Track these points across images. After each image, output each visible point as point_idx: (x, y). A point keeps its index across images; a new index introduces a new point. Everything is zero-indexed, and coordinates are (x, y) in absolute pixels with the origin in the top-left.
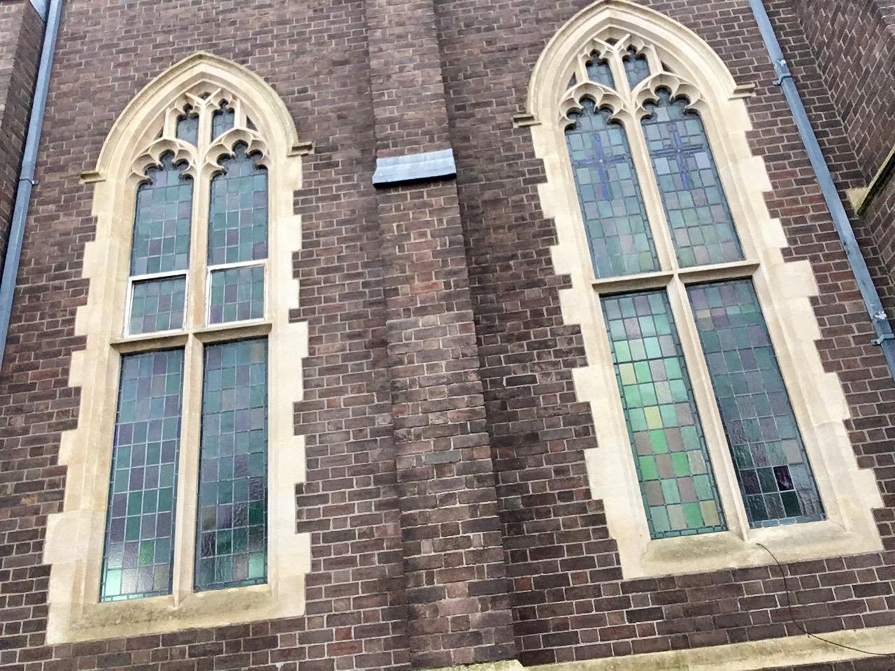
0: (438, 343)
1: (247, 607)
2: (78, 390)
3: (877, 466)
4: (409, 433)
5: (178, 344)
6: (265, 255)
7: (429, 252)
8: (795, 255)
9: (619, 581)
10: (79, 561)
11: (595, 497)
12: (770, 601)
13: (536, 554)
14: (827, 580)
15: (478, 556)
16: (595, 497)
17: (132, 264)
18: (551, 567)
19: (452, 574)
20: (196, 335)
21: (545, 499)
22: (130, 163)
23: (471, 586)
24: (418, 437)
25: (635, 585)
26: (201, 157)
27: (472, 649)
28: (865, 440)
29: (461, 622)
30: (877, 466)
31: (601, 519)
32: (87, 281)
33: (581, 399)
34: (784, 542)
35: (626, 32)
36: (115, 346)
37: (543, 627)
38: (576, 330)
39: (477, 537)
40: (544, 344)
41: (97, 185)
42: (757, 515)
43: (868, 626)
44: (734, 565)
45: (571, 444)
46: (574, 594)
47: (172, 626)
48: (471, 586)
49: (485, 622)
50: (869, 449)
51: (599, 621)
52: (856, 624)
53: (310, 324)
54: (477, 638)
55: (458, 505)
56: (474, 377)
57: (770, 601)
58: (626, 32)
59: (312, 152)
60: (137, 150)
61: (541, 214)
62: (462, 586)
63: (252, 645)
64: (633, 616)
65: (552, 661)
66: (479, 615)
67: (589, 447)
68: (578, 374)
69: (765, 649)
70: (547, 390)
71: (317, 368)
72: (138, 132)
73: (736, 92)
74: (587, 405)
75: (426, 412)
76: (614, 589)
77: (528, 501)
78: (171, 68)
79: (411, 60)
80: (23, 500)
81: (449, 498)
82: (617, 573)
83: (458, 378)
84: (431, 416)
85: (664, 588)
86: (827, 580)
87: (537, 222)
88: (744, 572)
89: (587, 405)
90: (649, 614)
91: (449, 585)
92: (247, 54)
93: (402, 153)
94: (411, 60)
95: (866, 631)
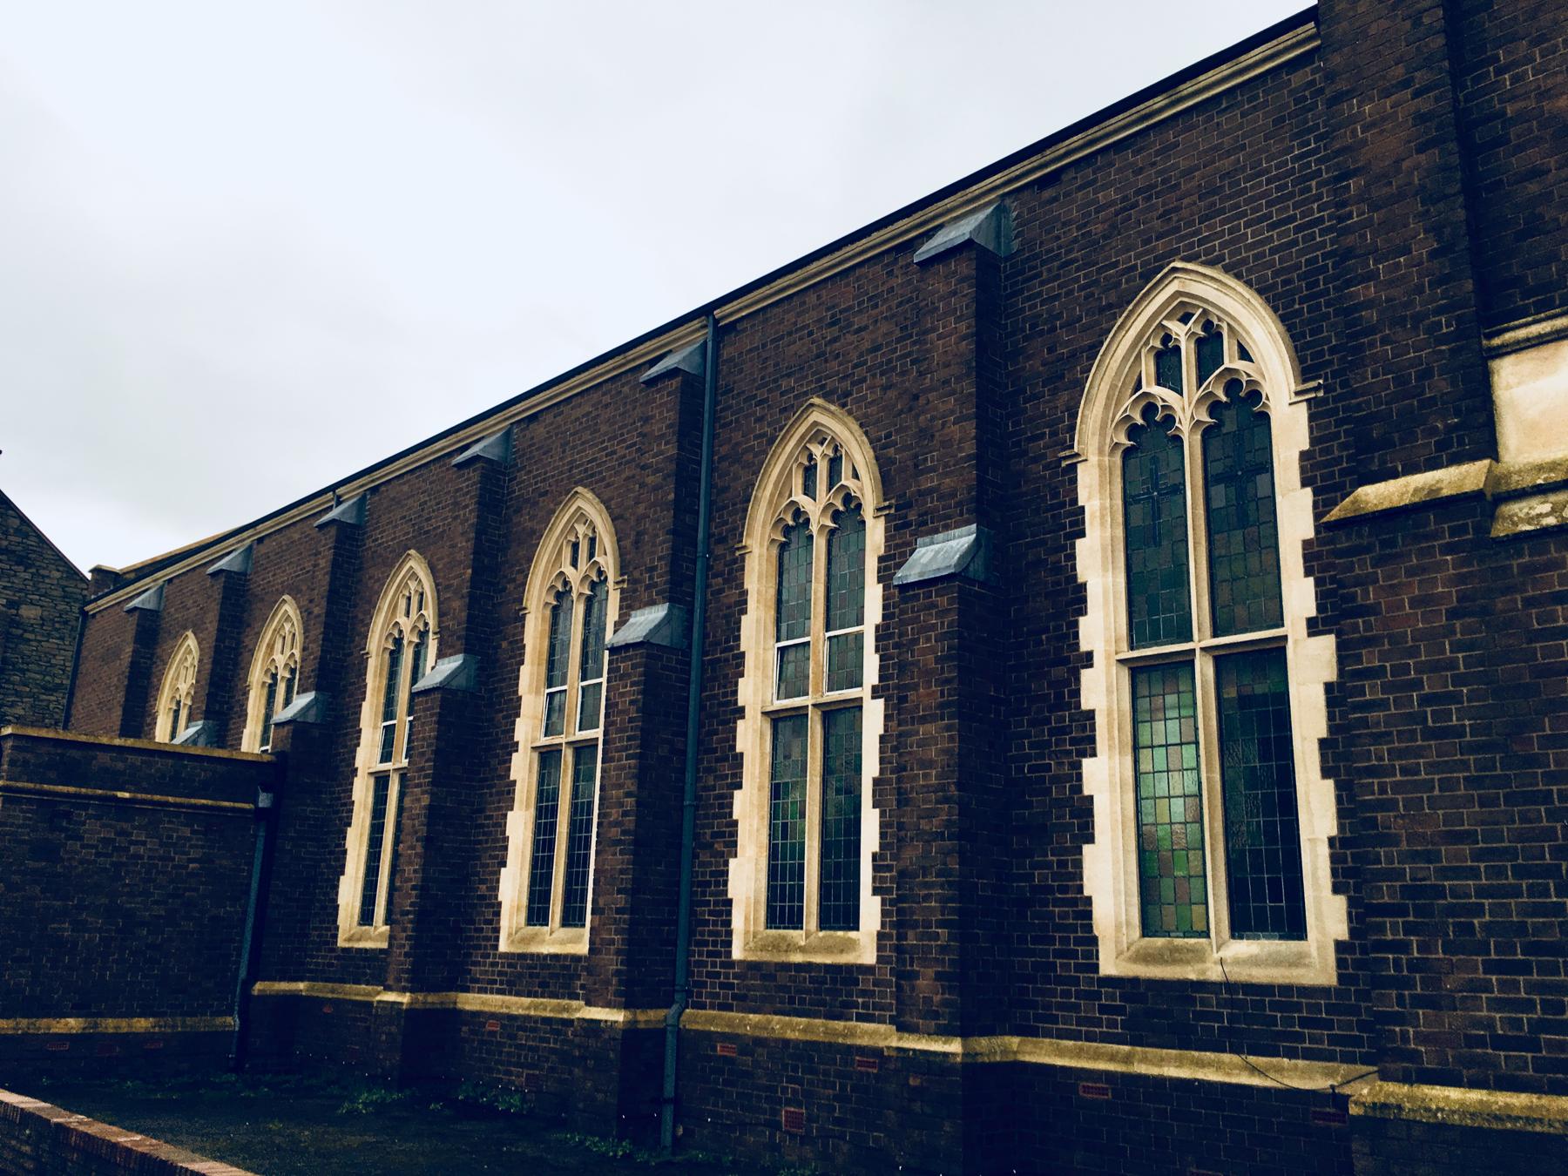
0: (932, 753)
1: (842, 951)
2: (742, 754)
3: (1352, 893)
4: (906, 835)
6: (863, 624)
7: (931, 657)
8: (1321, 628)
9: (1096, 976)
10: (748, 898)
11: (1086, 893)
12: (1218, 1017)
13: (1035, 940)
14: (1276, 1006)
15: (943, 949)
16: (1086, 893)
17: (778, 631)
18: (1045, 953)
19: (925, 961)
20: (814, 705)
21: (1050, 890)
22: (769, 528)
23: (937, 973)
24: (912, 839)
25: (1111, 981)
27: (933, 1023)
28: (1346, 862)
29: (928, 1000)
30: (1352, 893)
32: (744, 653)
33: (1086, 792)
34: (1254, 961)
35: (1199, 307)
36: (765, 714)
37: (1034, 1005)
38: (1091, 715)
40: (1063, 731)
41: (747, 556)
42: (1241, 927)
43: (1305, 1058)
44: (1193, 976)
45: (1074, 837)
46: (1060, 980)
47: (798, 958)
48: (937, 973)
49: (945, 1003)
50: (1348, 873)
51: (1076, 1008)
52: (1292, 1054)
53: (886, 701)
55: (933, 904)
56: (953, 788)
57: (1218, 1017)
58: (1199, 307)
59: (893, 511)
60: (774, 512)
61: (1075, 576)
62: (931, 972)
63: (845, 982)
65: (1037, 1035)
66: (939, 997)
67: (1088, 843)
68: (1087, 764)
69: (1202, 1061)
70: (1057, 779)
71: (889, 745)
72: (772, 495)
73: (1297, 393)
74: (1091, 798)
75: (920, 818)
76: (1090, 981)
77: (1034, 889)
78: (793, 419)
79: (952, 412)
80: (716, 846)
81: (927, 898)
82: (1095, 968)
83: (943, 788)
84: (921, 821)
85: (1128, 986)
86: (1276, 1006)
87: (1070, 587)
88: (1202, 985)
89: (1091, 798)
90: (1118, 1010)
91: (922, 970)
92: (847, 394)
94: (952, 412)
95: (1300, 1063)
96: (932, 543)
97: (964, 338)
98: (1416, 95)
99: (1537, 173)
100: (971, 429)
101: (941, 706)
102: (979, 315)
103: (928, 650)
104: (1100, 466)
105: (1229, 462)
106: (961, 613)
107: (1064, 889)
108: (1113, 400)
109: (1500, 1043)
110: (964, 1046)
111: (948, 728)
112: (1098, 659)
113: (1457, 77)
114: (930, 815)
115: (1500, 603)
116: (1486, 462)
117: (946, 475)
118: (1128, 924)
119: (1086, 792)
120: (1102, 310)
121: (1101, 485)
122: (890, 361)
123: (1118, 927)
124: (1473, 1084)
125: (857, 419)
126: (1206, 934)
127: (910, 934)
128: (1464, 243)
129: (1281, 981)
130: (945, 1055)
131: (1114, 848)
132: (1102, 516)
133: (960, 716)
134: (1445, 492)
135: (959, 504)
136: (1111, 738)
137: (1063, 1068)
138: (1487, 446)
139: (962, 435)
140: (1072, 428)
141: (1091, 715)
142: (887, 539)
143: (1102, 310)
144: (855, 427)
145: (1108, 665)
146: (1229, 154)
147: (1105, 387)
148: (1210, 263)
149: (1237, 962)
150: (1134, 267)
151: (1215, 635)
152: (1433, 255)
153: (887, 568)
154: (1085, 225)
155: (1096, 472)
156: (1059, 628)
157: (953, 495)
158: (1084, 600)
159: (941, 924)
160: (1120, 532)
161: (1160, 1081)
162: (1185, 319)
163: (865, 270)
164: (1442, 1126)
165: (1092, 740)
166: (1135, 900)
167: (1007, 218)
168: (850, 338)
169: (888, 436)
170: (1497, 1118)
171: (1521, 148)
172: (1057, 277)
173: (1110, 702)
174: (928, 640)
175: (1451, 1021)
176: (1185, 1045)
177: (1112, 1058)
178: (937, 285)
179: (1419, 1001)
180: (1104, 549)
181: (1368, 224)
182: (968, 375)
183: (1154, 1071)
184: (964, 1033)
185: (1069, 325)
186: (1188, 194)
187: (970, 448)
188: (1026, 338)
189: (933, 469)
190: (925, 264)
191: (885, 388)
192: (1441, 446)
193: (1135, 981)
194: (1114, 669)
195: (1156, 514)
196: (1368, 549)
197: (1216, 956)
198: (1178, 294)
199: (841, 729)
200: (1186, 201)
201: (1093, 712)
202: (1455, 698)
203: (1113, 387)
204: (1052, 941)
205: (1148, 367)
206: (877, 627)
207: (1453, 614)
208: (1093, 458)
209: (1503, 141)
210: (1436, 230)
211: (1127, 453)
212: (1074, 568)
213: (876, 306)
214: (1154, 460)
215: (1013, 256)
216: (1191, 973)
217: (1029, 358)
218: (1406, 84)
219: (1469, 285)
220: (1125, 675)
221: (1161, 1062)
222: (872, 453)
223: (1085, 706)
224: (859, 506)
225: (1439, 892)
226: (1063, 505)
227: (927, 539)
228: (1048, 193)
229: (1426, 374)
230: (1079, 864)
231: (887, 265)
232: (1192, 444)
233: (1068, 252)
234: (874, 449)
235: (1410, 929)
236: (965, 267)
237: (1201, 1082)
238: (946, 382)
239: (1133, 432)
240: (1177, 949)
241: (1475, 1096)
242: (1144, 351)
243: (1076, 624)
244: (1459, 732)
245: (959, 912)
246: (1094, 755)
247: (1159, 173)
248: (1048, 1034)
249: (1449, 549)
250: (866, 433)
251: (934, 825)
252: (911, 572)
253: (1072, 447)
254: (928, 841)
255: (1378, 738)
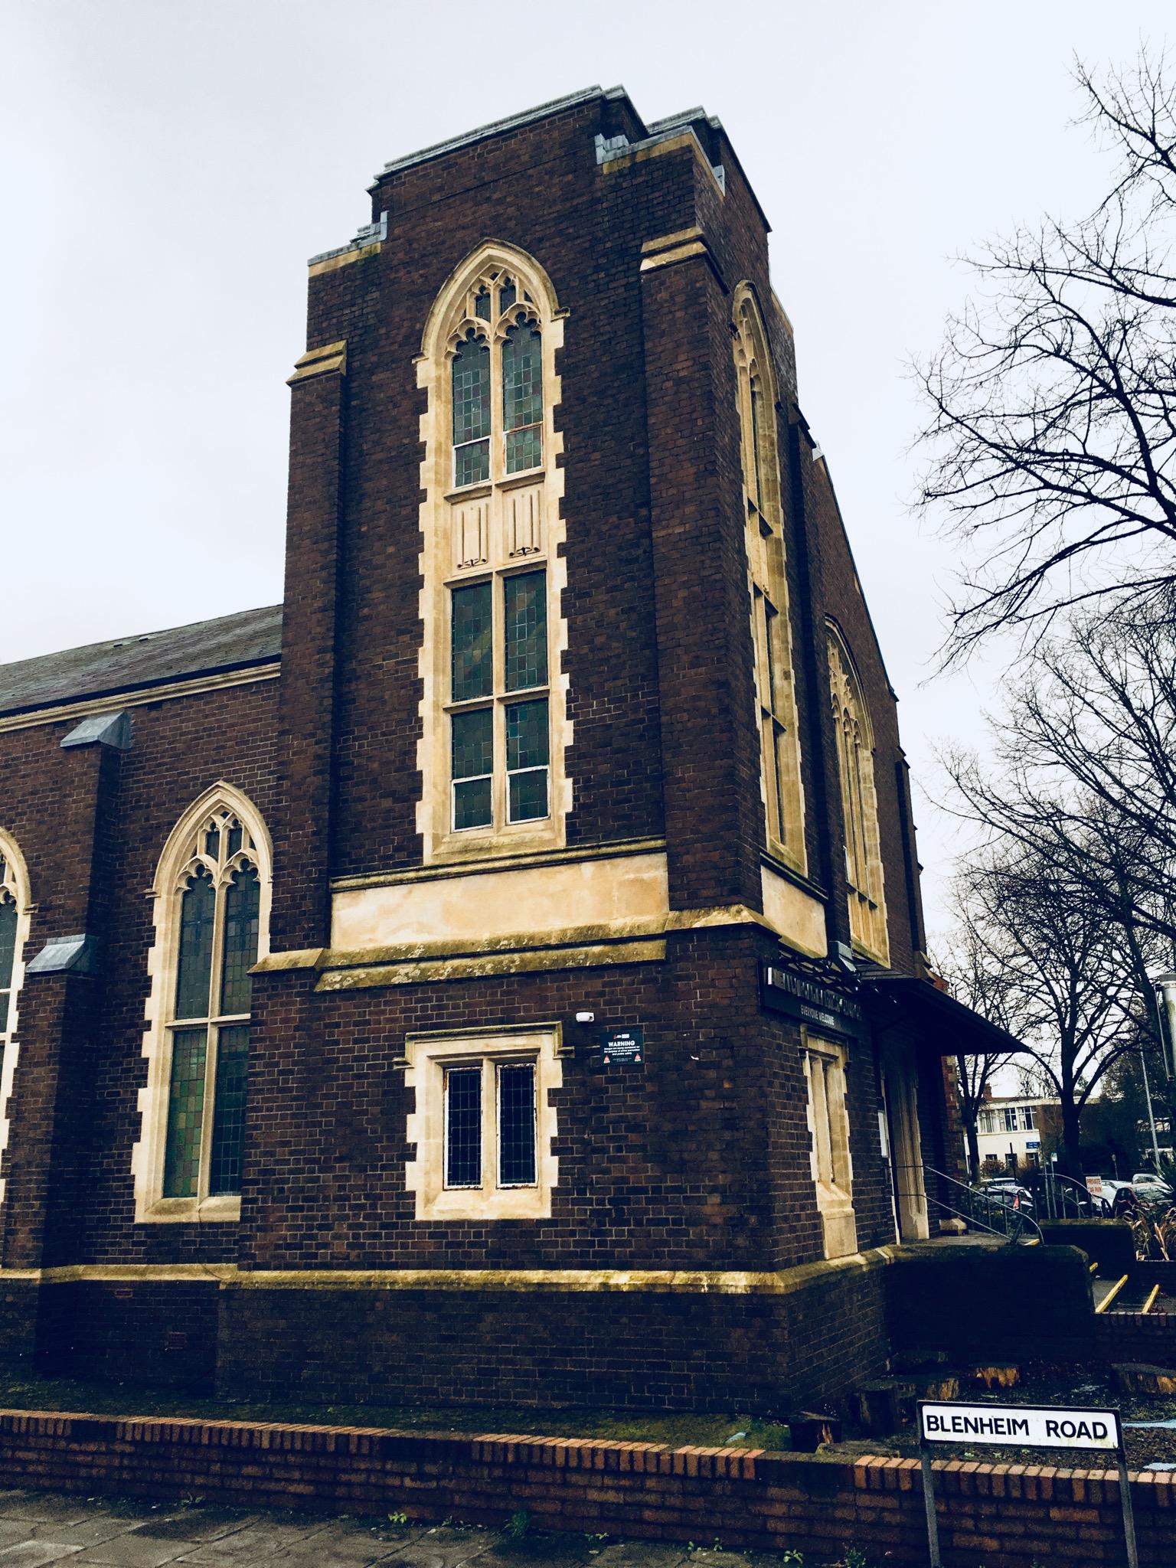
5: (541, 568)
14: (224, 1234)
15: (36, 1214)
21: (110, 1171)
25: (142, 1226)
26: (491, 329)
29: (23, 1247)
31: (132, 1187)
33: (139, 1110)
34: (217, 1209)
37: (94, 1244)
39: (37, 1203)
40: (129, 1070)
44: (184, 1220)
54: (27, 1256)
56: (52, 1110)
61: (146, 971)
64: (135, 1244)
68: (141, 1091)
70: (122, 1101)
81: (29, 1181)
82: (132, 1219)
88: (188, 1225)
93: (60, 936)
96: (56, 943)
97: (90, 806)
98: (317, 743)
99: (362, 799)
100: (88, 869)
101: (50, 1056)
102: (100, 792)
103: (45, 1018)
104: (168, 900)
105: (240, 909)
106: (67, 994)
107: (120, 1171)
108: (179, 860)
109: (289, 1247)
110: (42, 1273)
111: (52, 1071)
112: (154, 1026)
113: (335, 739)
114: (36, 1127)
115: (315, 1025)
116: (320, 950)
117: (69, 898)
118: (155, 1191)
119: (139, 1110)
120: (178, 801)
121: (167, 915)
122: (43, 804)
123: (148, 1193)
124: (276, 1268)
125: (18, 840)
126: (195, 1195)
127: (17, 1205)
128: (326, 831)
129: (227, 1220)
130: (30, 1280)
131: (151, 1146)
132: (166, 934)
133: (61, 1063)
134: (300, 965)
135: (75, 919)
136: (156, 1076)
137: (107, 1282)
138: (325, 940)
139: (82, 871)
140: (153, 874)
141: (147, 1060)
142: (32, 931)
143: (178, 801)
144: (16, 847)
145: (160, 1028)
146: (254, 721)
147: (175, 851)
148: (238, 786)
149: (209, 1210)
150: (197, 778)
151: (222, 1014)
152: (314, 833)
153: (29, 951)
154: (173, 742)
155: (164, 906)
156: (133, 1004)
157: (72, 912)
158: (149, 987)
159: (36, 1198)
160: (176, 945)
161: (159, 1283)
162: (225, 815)
163: (31, 733)
164: (257, 1291)
165: (145, 1077)
166: (161, 1175)
167: (128, 723)
168: (19, 781)
169: (38, 857)
170: (279, 1284)
171: (357, 784)
172: (153, 772)
173: (158, 1053)
174: (45, 1011)
175: (272, 1236)
176: (176, 1261)
177: (136, 1272)
178: (74, 764)
179: (259, 1229)
180: (165, 954)
181: (288, 808)
182: (89, 832)
183: (157, 1278)
184: (44, 1265)
185: (158, 805)
186: (230, 740)
187: (86, 882)
188: (133, 808)
189: (62, 892)
190: (68, 749)
191: (40, 823)
192: (306, 937)
193: (153, 1225)
194: (163, 1032)
195: (198, 935)
196: (266, 990)
197: (198, 1207)
198: (219, 801)
199: (213, 839)
200: (229, 744)
201: (148, 1059)
202: (291, 1072)
203: (180, 851)
204: (109, 1203)
205: (201, 842)
206: (19, 993)
207: (296, 1029)
208: (164, 896)
209: (349, 778)
210: (316, 819)
211: (186, 894)
212: (146, 966)
213: (37, 761)
214: (201, 901)
215: (129, 750)
216: (183, 1218)
217: (132, 822)
218: (313, 735)
219: (326, 854)
220: (170, 1036)
221: (161, 1272)
222: (26, 868)
223: (144, 1055)
224: (15, 902)
225: (273, 1172)
226: (144, 924)
227: (54, 940)
228: (154, 714)
229: (303, 898)
230: (130, 1155)
231: (48, 734)
232: (221, 895)
233: (163, 757)
234: (28, 864)
235: (260, 1192)
236: (93, 757)
237: (180, 1281)
238: (74, 834)
239: (190, 881)
240: (179, 1205)
241: (424, 1274)
242: (200, 831)
243: (143, 1002)
244: (290, 1090)
245: (48, 1190)
246: (146, 1086)
247: (217, 721)
248: (102, 1262)
249: (298, 994)
250: (23, 852)
251: (38, 1134)
252: (39, 964)
253: (151, 887)
254: (33, 1145)
255: (259, 1091)
